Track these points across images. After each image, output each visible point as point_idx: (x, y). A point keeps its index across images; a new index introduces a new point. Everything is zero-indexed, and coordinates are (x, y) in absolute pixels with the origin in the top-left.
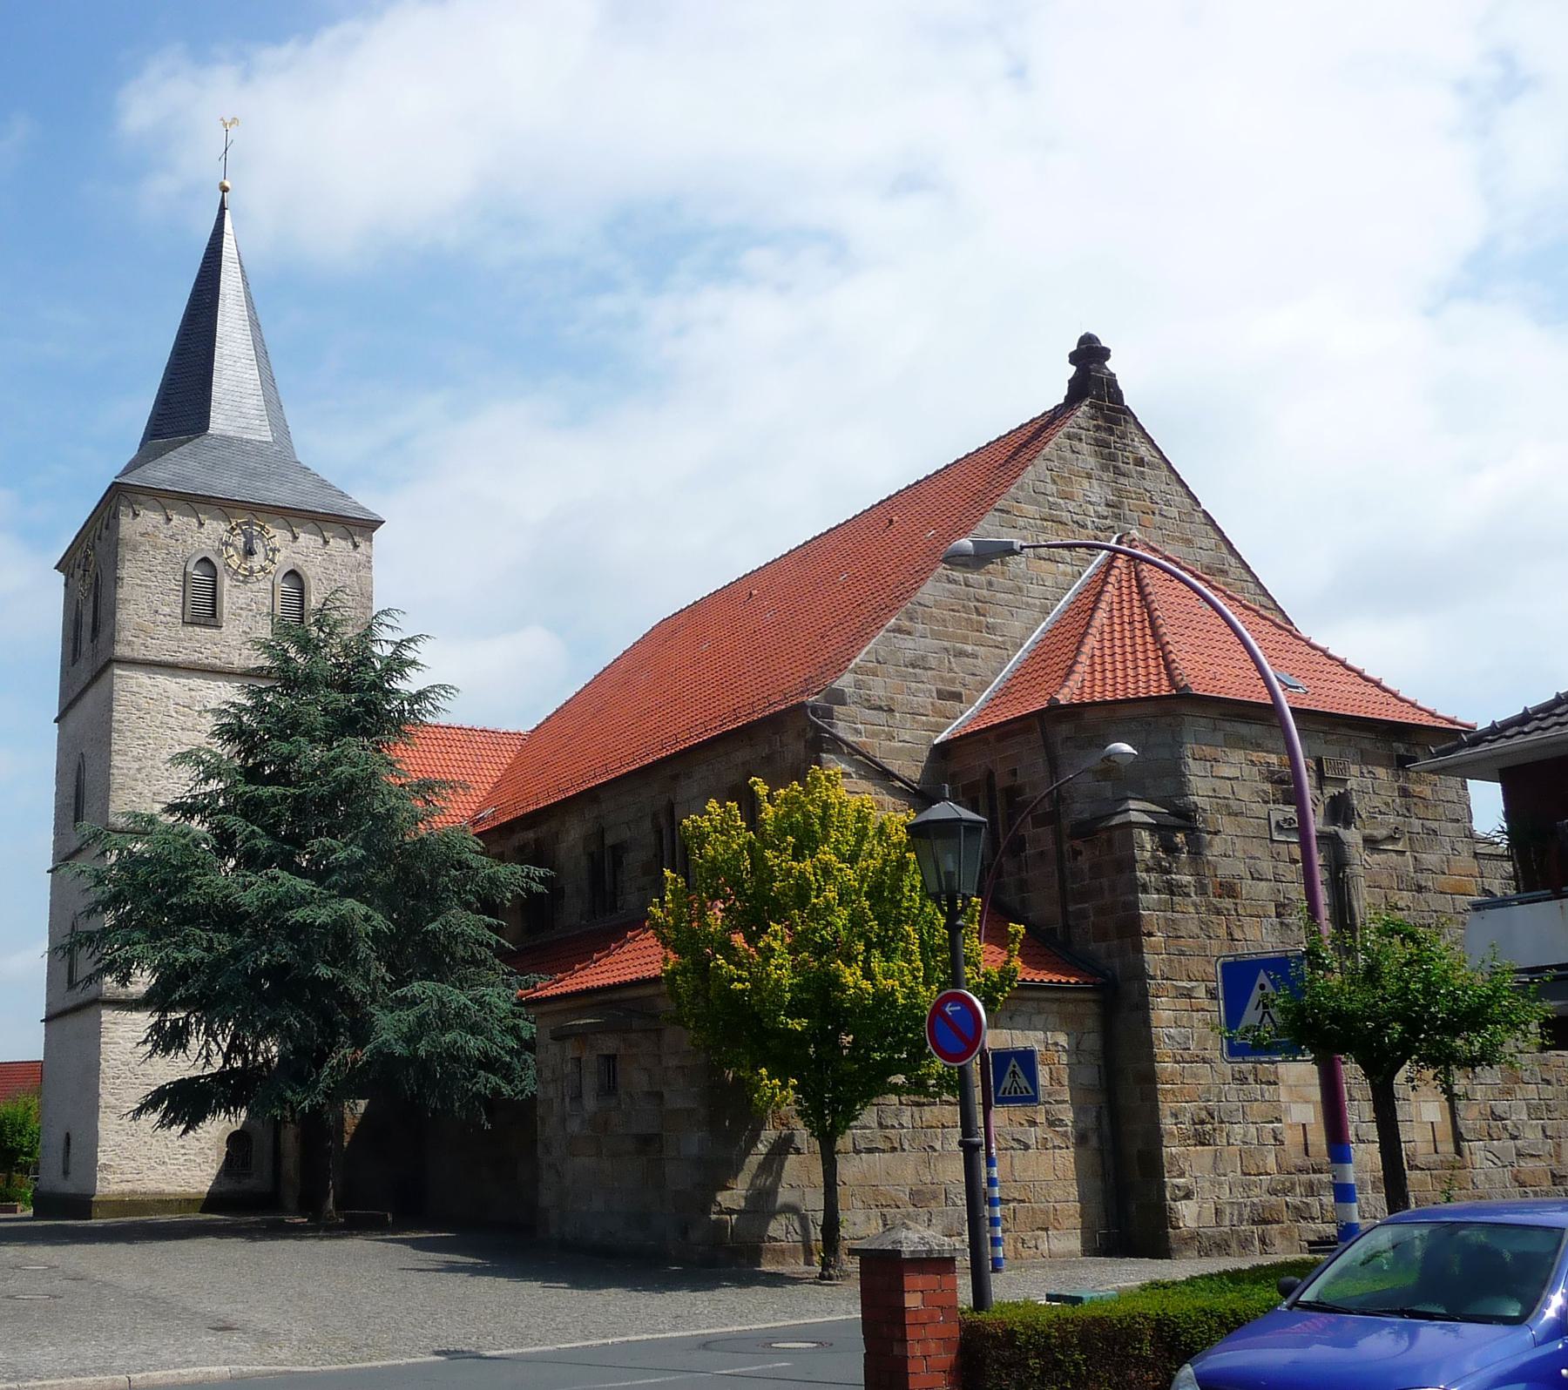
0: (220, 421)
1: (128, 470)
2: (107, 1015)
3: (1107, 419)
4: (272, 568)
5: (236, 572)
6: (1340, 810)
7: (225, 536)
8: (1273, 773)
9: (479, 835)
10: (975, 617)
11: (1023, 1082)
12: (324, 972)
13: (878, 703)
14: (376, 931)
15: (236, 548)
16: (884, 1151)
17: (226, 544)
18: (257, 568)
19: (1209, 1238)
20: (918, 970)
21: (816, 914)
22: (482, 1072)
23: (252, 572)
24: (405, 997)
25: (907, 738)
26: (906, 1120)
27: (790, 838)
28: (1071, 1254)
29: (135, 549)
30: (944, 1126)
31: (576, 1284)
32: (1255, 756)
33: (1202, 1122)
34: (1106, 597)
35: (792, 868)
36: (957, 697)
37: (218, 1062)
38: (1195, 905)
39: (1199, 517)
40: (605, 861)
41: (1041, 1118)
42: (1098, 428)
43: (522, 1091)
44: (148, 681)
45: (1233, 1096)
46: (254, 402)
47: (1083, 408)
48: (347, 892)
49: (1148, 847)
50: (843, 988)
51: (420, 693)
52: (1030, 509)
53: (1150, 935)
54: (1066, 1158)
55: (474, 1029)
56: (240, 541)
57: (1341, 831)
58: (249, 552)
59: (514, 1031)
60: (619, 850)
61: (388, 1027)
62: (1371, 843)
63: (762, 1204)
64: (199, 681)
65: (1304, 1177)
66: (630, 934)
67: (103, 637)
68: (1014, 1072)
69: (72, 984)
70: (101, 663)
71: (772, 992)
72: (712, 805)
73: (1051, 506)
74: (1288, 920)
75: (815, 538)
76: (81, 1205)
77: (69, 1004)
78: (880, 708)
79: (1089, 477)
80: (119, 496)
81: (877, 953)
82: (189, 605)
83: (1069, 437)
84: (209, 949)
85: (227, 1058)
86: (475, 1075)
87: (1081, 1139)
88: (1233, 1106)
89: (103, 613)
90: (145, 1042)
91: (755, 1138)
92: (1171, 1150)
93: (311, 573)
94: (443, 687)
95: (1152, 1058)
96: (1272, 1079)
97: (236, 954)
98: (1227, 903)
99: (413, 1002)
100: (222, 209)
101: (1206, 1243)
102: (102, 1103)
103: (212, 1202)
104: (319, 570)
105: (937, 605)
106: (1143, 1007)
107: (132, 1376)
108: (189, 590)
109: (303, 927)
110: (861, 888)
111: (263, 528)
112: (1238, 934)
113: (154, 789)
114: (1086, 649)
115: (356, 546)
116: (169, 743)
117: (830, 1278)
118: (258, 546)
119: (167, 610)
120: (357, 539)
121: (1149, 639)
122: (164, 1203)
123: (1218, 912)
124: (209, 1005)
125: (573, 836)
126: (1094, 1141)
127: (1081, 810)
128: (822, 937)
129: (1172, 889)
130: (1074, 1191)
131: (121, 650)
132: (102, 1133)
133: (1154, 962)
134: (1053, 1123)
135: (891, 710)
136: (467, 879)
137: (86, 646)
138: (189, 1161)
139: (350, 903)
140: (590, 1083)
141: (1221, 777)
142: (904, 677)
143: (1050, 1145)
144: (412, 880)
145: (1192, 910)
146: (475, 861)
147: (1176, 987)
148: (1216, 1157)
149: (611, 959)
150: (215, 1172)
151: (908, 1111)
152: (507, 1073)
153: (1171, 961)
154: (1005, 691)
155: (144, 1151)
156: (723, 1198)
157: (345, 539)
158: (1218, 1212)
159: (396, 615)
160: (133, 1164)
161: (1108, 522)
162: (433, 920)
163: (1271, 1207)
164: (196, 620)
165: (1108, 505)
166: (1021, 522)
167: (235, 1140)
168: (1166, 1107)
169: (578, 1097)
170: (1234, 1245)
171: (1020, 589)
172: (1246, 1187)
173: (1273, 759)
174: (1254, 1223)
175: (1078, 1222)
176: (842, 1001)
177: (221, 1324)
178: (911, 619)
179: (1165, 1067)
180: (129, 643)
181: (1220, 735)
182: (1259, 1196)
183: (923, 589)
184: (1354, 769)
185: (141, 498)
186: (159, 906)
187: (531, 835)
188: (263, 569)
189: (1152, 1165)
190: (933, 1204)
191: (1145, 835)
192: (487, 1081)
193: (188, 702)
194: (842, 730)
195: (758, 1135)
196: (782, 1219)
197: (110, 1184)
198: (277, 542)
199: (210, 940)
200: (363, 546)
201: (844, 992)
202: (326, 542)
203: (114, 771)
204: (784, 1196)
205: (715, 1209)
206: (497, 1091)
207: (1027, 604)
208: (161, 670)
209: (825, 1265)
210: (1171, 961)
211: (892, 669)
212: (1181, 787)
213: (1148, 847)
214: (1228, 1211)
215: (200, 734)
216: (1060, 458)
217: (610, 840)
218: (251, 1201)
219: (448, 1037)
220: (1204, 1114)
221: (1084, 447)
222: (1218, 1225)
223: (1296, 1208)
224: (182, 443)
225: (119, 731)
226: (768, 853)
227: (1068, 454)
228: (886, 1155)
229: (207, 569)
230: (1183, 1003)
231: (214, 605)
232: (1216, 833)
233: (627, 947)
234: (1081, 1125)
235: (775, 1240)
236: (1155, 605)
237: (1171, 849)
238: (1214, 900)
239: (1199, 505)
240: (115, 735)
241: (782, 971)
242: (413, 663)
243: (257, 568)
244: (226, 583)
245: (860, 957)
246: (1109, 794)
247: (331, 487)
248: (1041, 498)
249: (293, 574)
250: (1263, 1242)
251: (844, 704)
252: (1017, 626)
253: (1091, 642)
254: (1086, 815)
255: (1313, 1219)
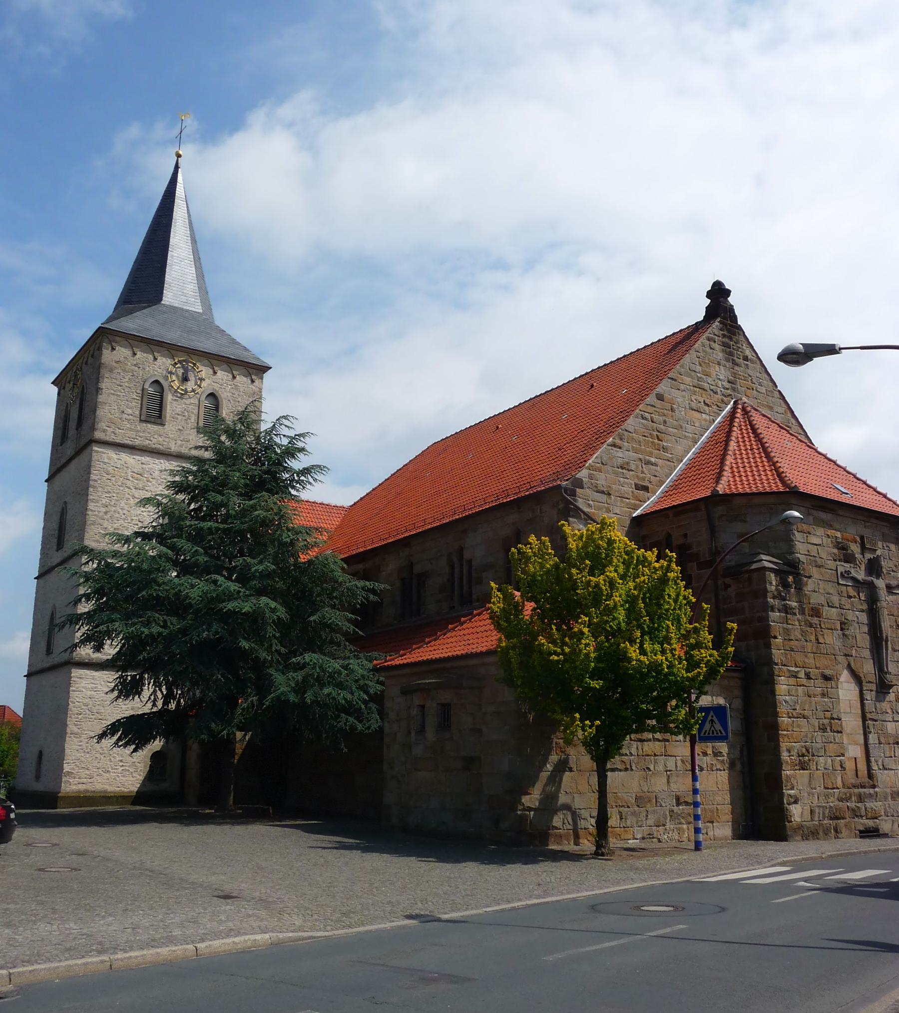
0: (169, 297)
1: (109, 320)
2: (76, 673)
3: (728, 331)
4: (200, 390)
5: (176, 391)
6: (874, 567)
7: (171, 368)
8: (838, 543)
9: (342, 560)
10: (656, 441)
11: (718, 726)
12: (245, 644)
13: (602, 489)
14: (279, 618)
15: (177, 376)
16: (620, 770)
17: (171, 373)
18: (189, 389)
19: (808, 828)
20: (675, 650)
21: (609, 611)
22: (343, 715)
23: (186, 391)
24: (298, 663)
25: (618, 512)
26: (634, 751)
27: (587, 562)
28: (726, 838)
29: (111, 371)
30: (655, 755)
31: (441, 859)
32: (830, 532)
33: (803, 755)
34: (734, 434)
35: (590, 581)
36: (646, 489)
37: (160, 704)
38: (798, 620)
39: (776, 394)
40: (412, 584)
41: (710, 751)
42: (724, 336)
43: (369, 728)
44: (115, 456)
45: (819, 740)
46: (191, 287)
47: (717, 323)
48: (260, 593)
49: (774, 583)
50: (629, 660)
51: (304, 469)
52: (687, 380)
53: (775, 637)
54: (723, 776)
55: (340, 686)
56: (180, 372)
57: (875, 580)
58: (185, 379)
59: (364, 689)
60: (422, 578)
61: (283, 684)
62: (889, 588)
63: (549, 805)
64: (148, 459)
65: (856, 791)
66: (450, 626)
67: (85, 427)
68: (712, 721)
69: (49, 651)
70: (83, 442)
71: (583, 661)
72: (532, 538)
73: (699, 379)
74: (847, 632)
75: (537, 396)
76: (51, 799)
77: (47, 665)
78: (603, 492)
79: (719, 364)
80: (103, 336)
81: (647, 637)
82: (144, 410)
83: (709, 339)
84: (165, 626)
85: (166, 703)
86: (339, 716)
87: (732, 765)
88: (819, 746)
89: (86, 410)
90: (113, 690)
91: (545, 761)
92: (787, 772)
93: (224, 395)
94: (319, 466)
95: (776, 714)
96: (839, 729)
97: (184, 632)
98: (815, 620)
99: (300, 667)
100: (177, 167)
101: (806, 832)
102: (68, 731)
103: (140, 798)
104: (229, 394)
105: (636, 432)
106: (770, 683)
107: (198, 945)
108: (145, 400)
109: (232, 613)
110: (639, 595)
111: (195, 364)
112: (821, 640)
113: (115, 526)
114: (728, 463)
115: (253, 381)
116: (129, 497)
117: (603, 855)
118: (191, 376)
119: (130, 411)
120: (254, 377)
121: (764, 459)
122: (107, 798)
123: (811, 626)
124: (153, 667)
125: (392, 565)
126: (738, 766)
127: (731, 560)
128: (611, 627)
129: (787, 610)
130: (728, 798)
131: (98, 435)
132: (67, 751)
133: (777, 654)
134: (716, 754)
135: (609, 494)
136: (334, 589)
137: (72, 431)
138: (122, 770)
139: (264, 600)
140: (431, 721)
141: (813, 543)
142: (616, 474)
143: (714, 768)
144: (301, 586)
145: (797, 623)
146: (339, 575)
147: (789, 671)
148: (811, 777)
149: (438, 642)
150: (142, 778)
151: (635, 744)
152: (358, 714)
153: (786, 654)
154: (675, 487)
155: (95, 763)
156: (525, 800)
157: (246, 376)
158: (812, 812)
159: (291, 419)
160: (87, 772)
161: (729, 392)
162: (312, 614)
163: (840, 809)
164: (148, 419)
165: (729, 382)
166: (682, 387)
167: (156, 757)
168: (784, 746)
169: (422, 730)
170: (821, 833)
171: (681, 427)
172: (826, 796)
173: (839, 534)
174: (831, 819)
175: (729, 817)
176: (628, 669)
177: (221, 894)
178: (621, 439)
179: (784, 720)
180: (104, 431)
181: (811, 518)
182: (833, 802)
183: (628, 421)
184: (880, 544)
185: (117, 338)
186: (128, 599)
187: (361, 566)
188: (193, 391)
189: (775, 782)
190: (649, 805)
191: (772, 575)
192: (346, 721)
193: (141, 471)
194: (581, 503)
195: (547, 759)
196: (561, 815)
197: (71, 785)
198: (203, 374)
199: (165, 621)
200: (257, 382)
201: (629, 662)
202: (234, 377)
203: (90, 513)
204: (563, 799)
205: (520, 807)
206: (353, 728)
207: (685, 436)
208: (126, 450)
209: (599, 846)
210: (786, 654)
211: (610, 468)
212: (791, 549)
213: (774, 583)
214: (817, 811)
215: (158, 487)
216: (704, 351)
217: (417, 569)
218: (163, 799)
219: (326, 691)
220: (804, 750)
221: (716, 346)
222: (812, 820)
223: (853, 810)
224: (145, 308)
225: (94, 487)
226: (574, 571)
227: (708, 349)
228: (622, 773)
229: (158, 389)
230: (792, 681)
231: (160, 411)
232: (810, 577)
233: (449, 635)
234: (731, 755)
235: (556, 828)
236: (765, 440)
237: (786, 586)
238: (809, 618)
239: (776, 386)
240: (91, 489)
241: (589, 646)
242: (302, 450)
243: (189, 389)
244: (169, 397)
245: (638, 641)
246: (747, 551)
247: (238, 344)
248: (693, 373)
249: (212, 396)
250: (836, 830)
251: (583, 488)
252: (679, 449)
253: (729, 460)
254: (733, 563)
255: (862, 817)
